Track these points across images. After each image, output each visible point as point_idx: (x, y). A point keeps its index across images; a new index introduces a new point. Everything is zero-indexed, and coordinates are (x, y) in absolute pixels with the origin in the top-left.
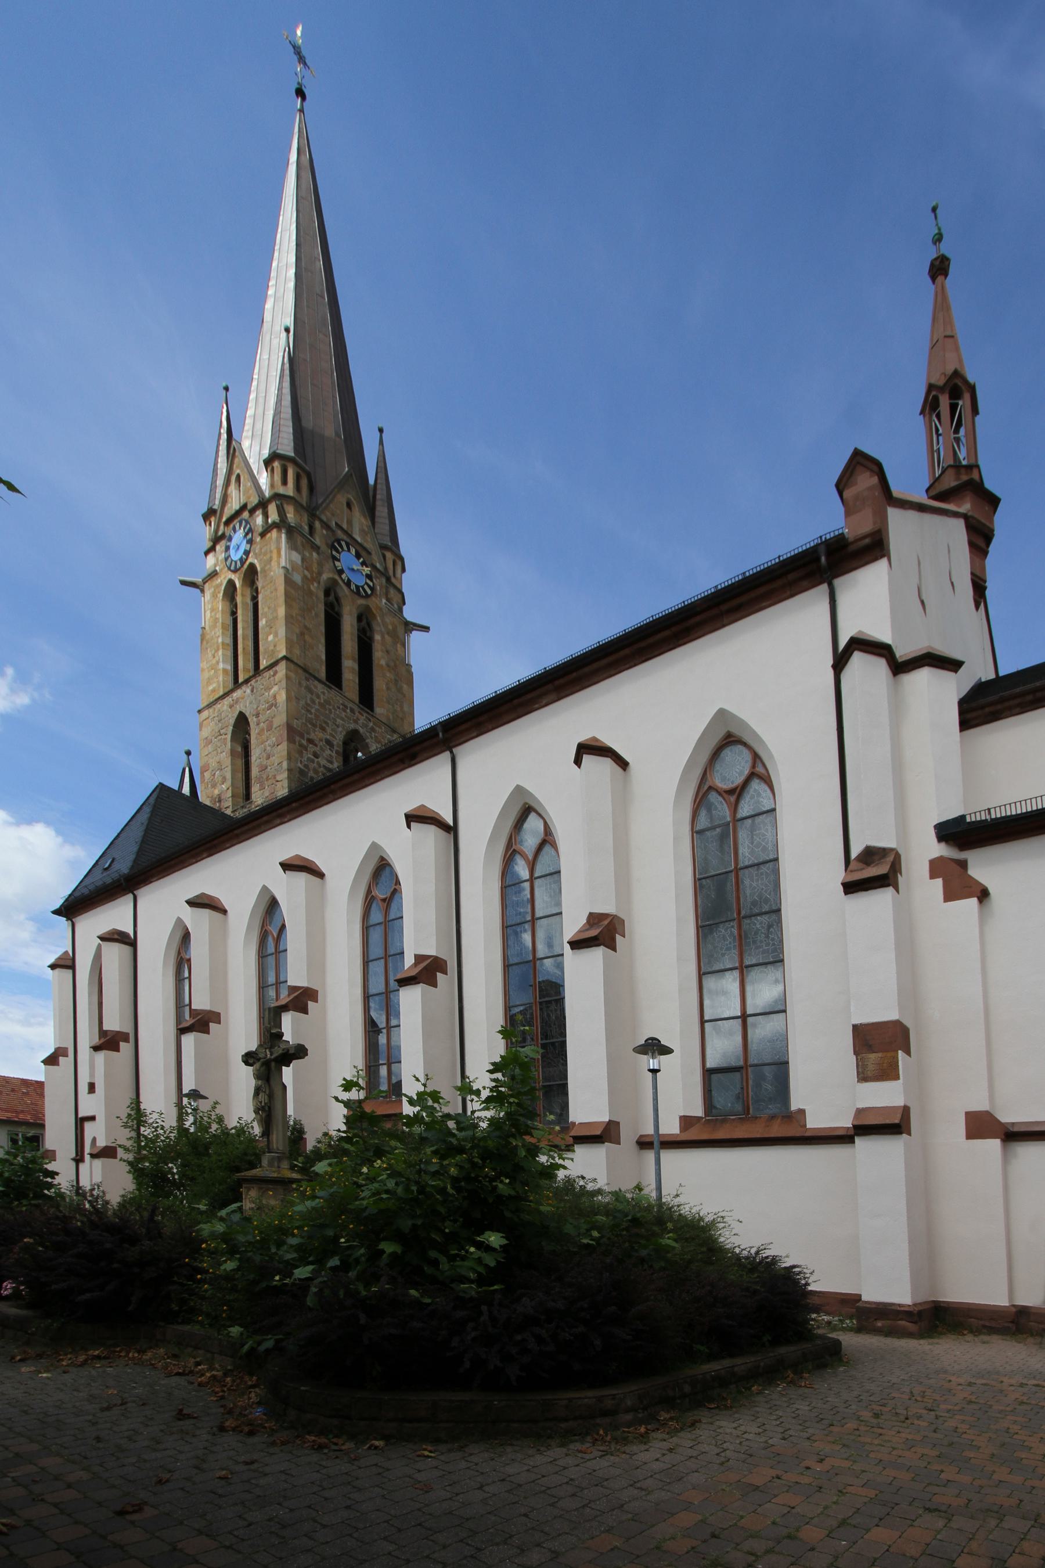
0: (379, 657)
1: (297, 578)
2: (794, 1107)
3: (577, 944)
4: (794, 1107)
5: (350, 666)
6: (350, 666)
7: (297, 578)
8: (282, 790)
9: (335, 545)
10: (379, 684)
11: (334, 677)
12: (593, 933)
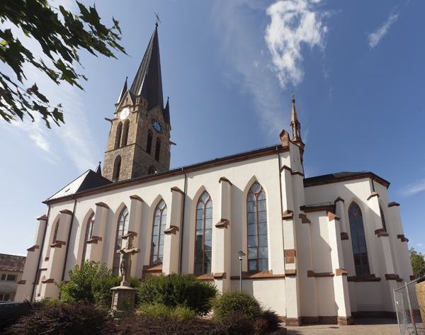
0: (162, 149)
1: (141, 125)
2: (371, 273)
3: (217, 226)
4: (371, 273)
5: (153, 149)
6: (153, 149)
7: (141, 125)
8: (129, 178)
9: (153, 121)
10: (161, 155)
11: (148, 151)
12: (222, 223)
